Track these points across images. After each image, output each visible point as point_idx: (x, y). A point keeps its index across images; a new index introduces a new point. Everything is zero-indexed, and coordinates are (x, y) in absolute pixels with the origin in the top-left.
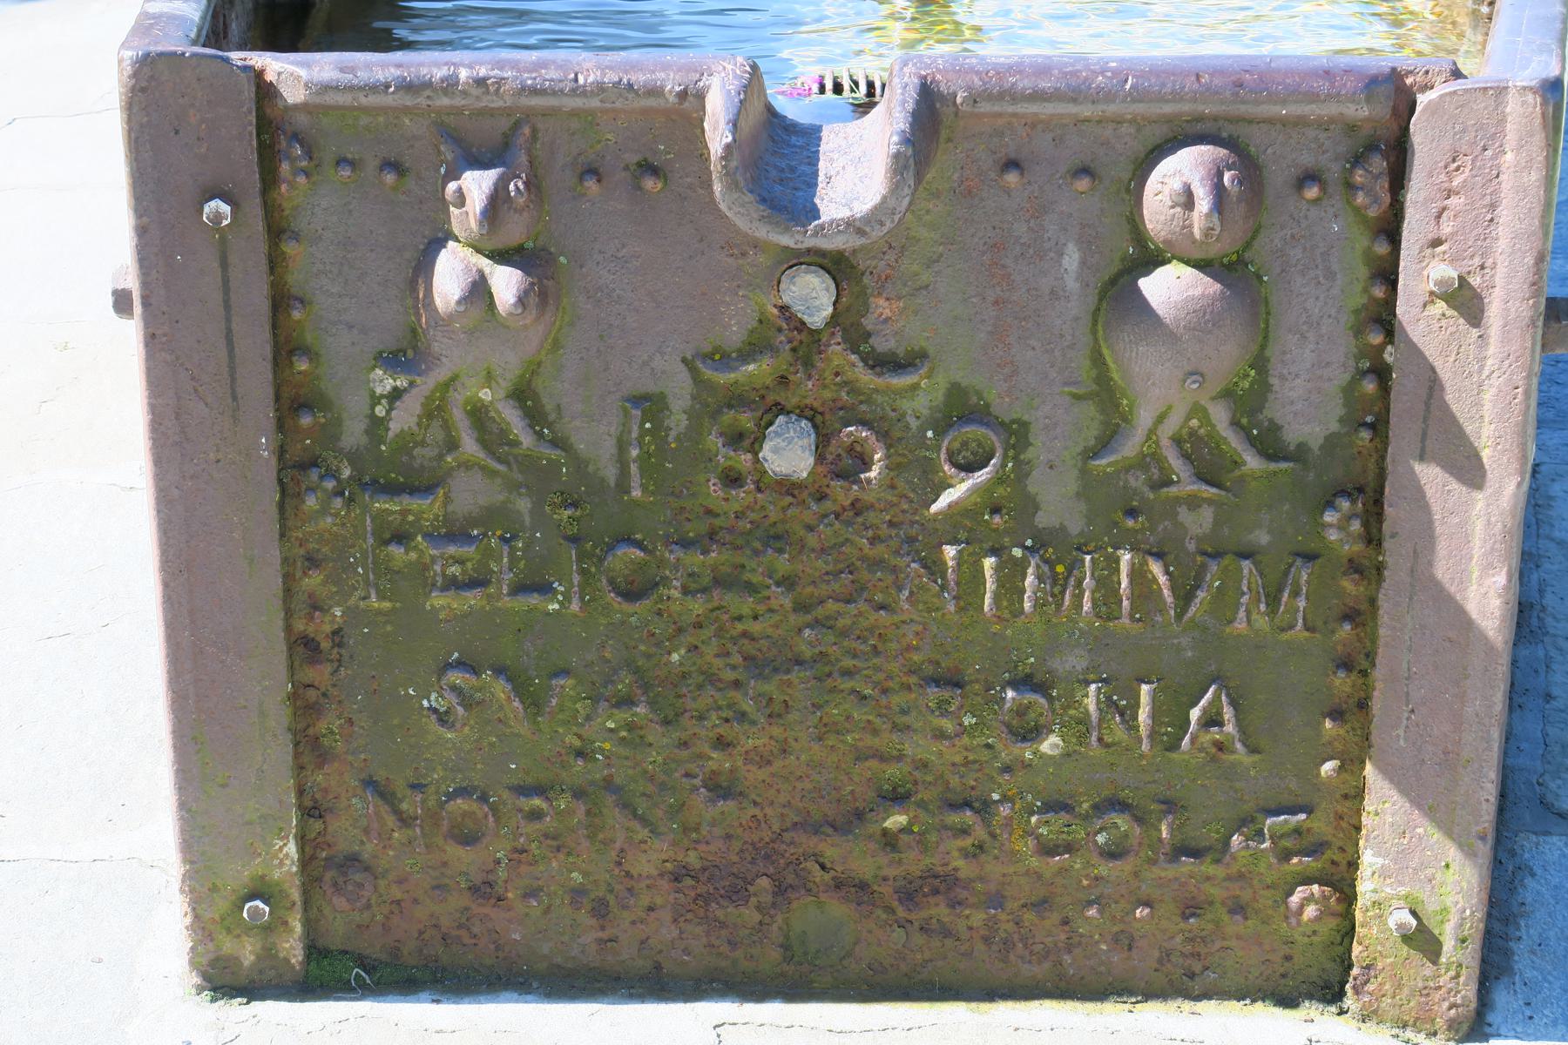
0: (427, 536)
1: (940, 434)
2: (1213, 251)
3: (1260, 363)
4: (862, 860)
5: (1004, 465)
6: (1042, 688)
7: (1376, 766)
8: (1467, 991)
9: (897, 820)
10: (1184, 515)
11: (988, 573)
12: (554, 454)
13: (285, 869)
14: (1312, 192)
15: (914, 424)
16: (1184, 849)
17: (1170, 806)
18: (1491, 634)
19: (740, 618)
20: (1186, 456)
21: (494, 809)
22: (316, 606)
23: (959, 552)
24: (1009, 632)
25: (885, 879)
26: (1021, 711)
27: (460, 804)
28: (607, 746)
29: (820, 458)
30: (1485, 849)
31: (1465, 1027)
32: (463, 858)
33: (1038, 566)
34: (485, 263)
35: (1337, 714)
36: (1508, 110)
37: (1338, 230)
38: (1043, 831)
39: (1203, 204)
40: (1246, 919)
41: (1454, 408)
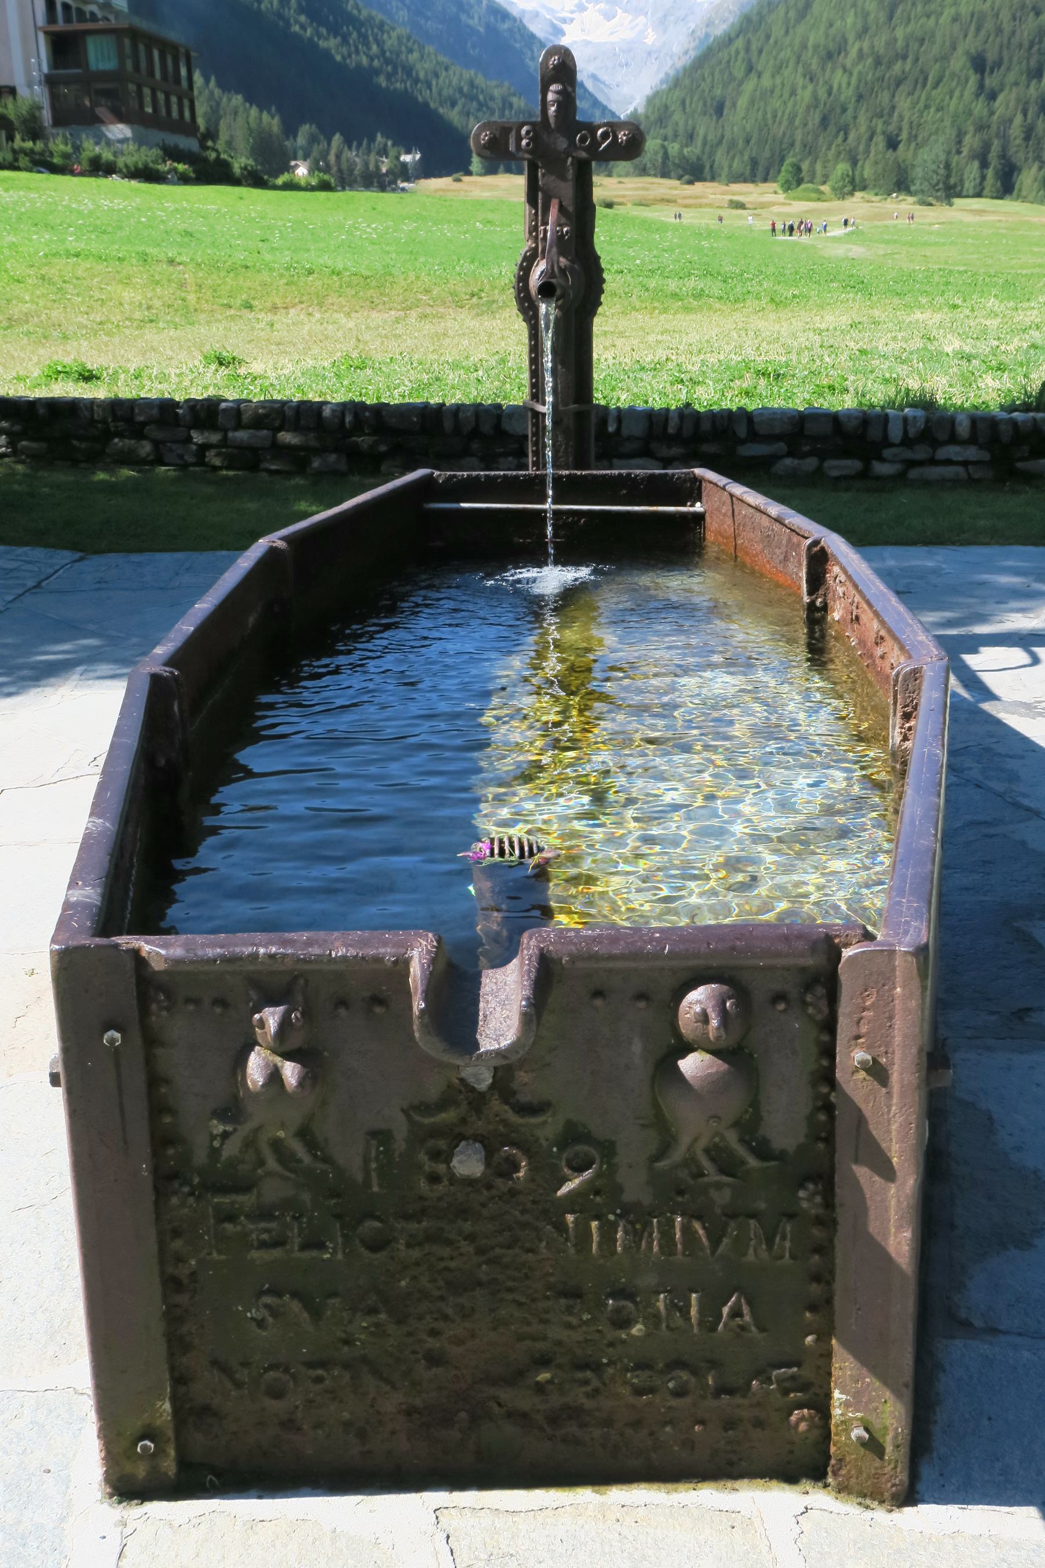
0: (247, 1216)
1: (562, 1148)
2: (722, 1044)
3: (755, 1104)
4: (522, 1400)
5: (601, 1167)
6: (631, 1297)
7: (838, 1340)
8: (902, 1476)
9: (544, 1376)
10: (713, 1194)
11: (594, 1231)
12: (324, 1167)
13: (163, 1418)
14: (781, 1006)
15: (544, 1143)
16: (723, 1390)
17: (714, 1364)
18: (904, 1266)
19: (442, 1259)
20: (713, 1159)
21: (294, 1377)
22: (179, 1259)
23: (576, 1219)
24: (608, 1264)
25: (538, 1411)
26: (618, 1310)
27: (272, 1374)
28: (363, 1337)
29: (488, 1164)
30: (908, 1393)
31: (902, 1498)
32: (274, 1406)
33: (625, 1226)
34: (278, 1060)
35: (813, 1308)
36: (897, 963)
37: (797, 1026)
38: (635, 1381)
39: (714, 1023)
40: (763, 1430)
41: (874, 1133)
